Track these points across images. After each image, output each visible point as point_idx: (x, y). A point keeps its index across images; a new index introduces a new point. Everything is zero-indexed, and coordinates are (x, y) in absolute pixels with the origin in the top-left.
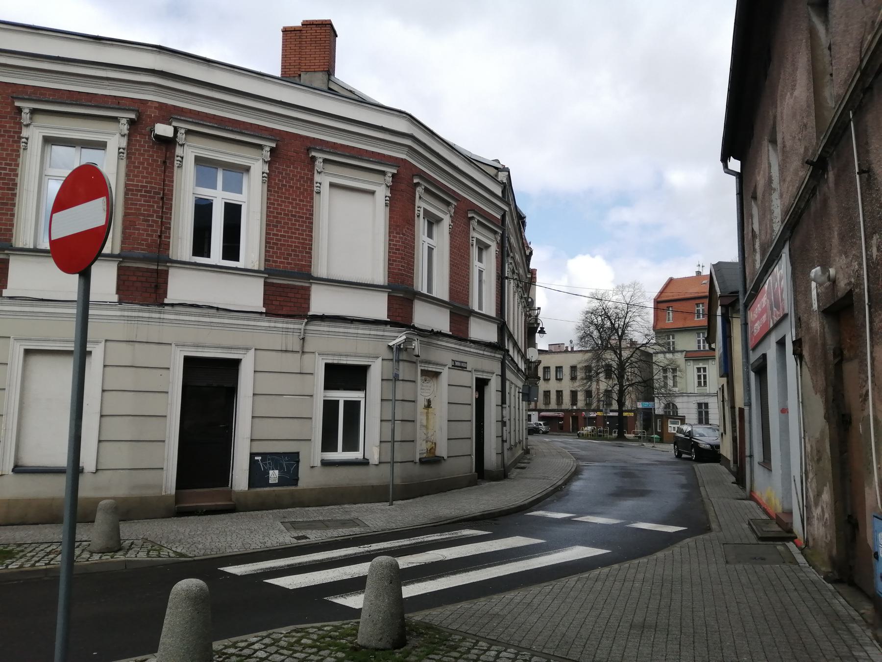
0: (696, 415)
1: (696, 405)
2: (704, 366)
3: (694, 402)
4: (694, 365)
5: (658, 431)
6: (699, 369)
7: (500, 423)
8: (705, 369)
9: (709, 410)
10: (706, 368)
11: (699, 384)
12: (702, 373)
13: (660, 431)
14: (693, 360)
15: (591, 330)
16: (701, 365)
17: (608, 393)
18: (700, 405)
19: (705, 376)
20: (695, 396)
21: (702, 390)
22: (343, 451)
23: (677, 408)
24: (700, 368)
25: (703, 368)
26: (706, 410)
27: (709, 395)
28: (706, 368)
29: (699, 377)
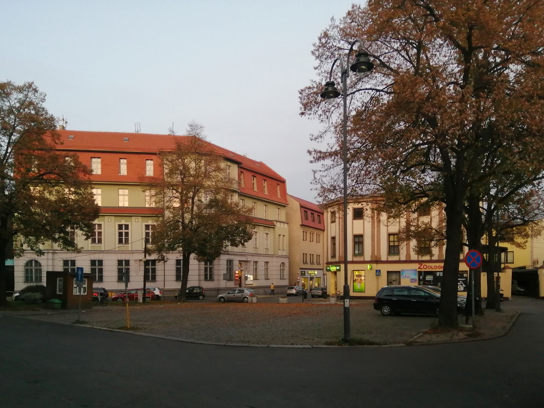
0: (23, 273)
1: (62, 262)
2: (127, 223)
3: (60, 259)
4: (142, 222)
5: (58, 293)
6: (120, 227)
7: (326, 151)
8: (127, 227)
9: (103, 267)
10: (128, 225)
11: (120, 241)
12: (124, 231)
13: (61, 293)
14: (115, 216)
15: (330, 54)
16: (123, 222)
17: (517, 229)
18: (120, 262)
19: (127, 234)
20: (116, 253)
21: (123, 247)
22: (128, 229)
23: (40, 265)
24: (149, 225)
25: (125, 225)
26: (126, 267)
27: (132, 252)
28: (128, 225)
29: (120, 234)
